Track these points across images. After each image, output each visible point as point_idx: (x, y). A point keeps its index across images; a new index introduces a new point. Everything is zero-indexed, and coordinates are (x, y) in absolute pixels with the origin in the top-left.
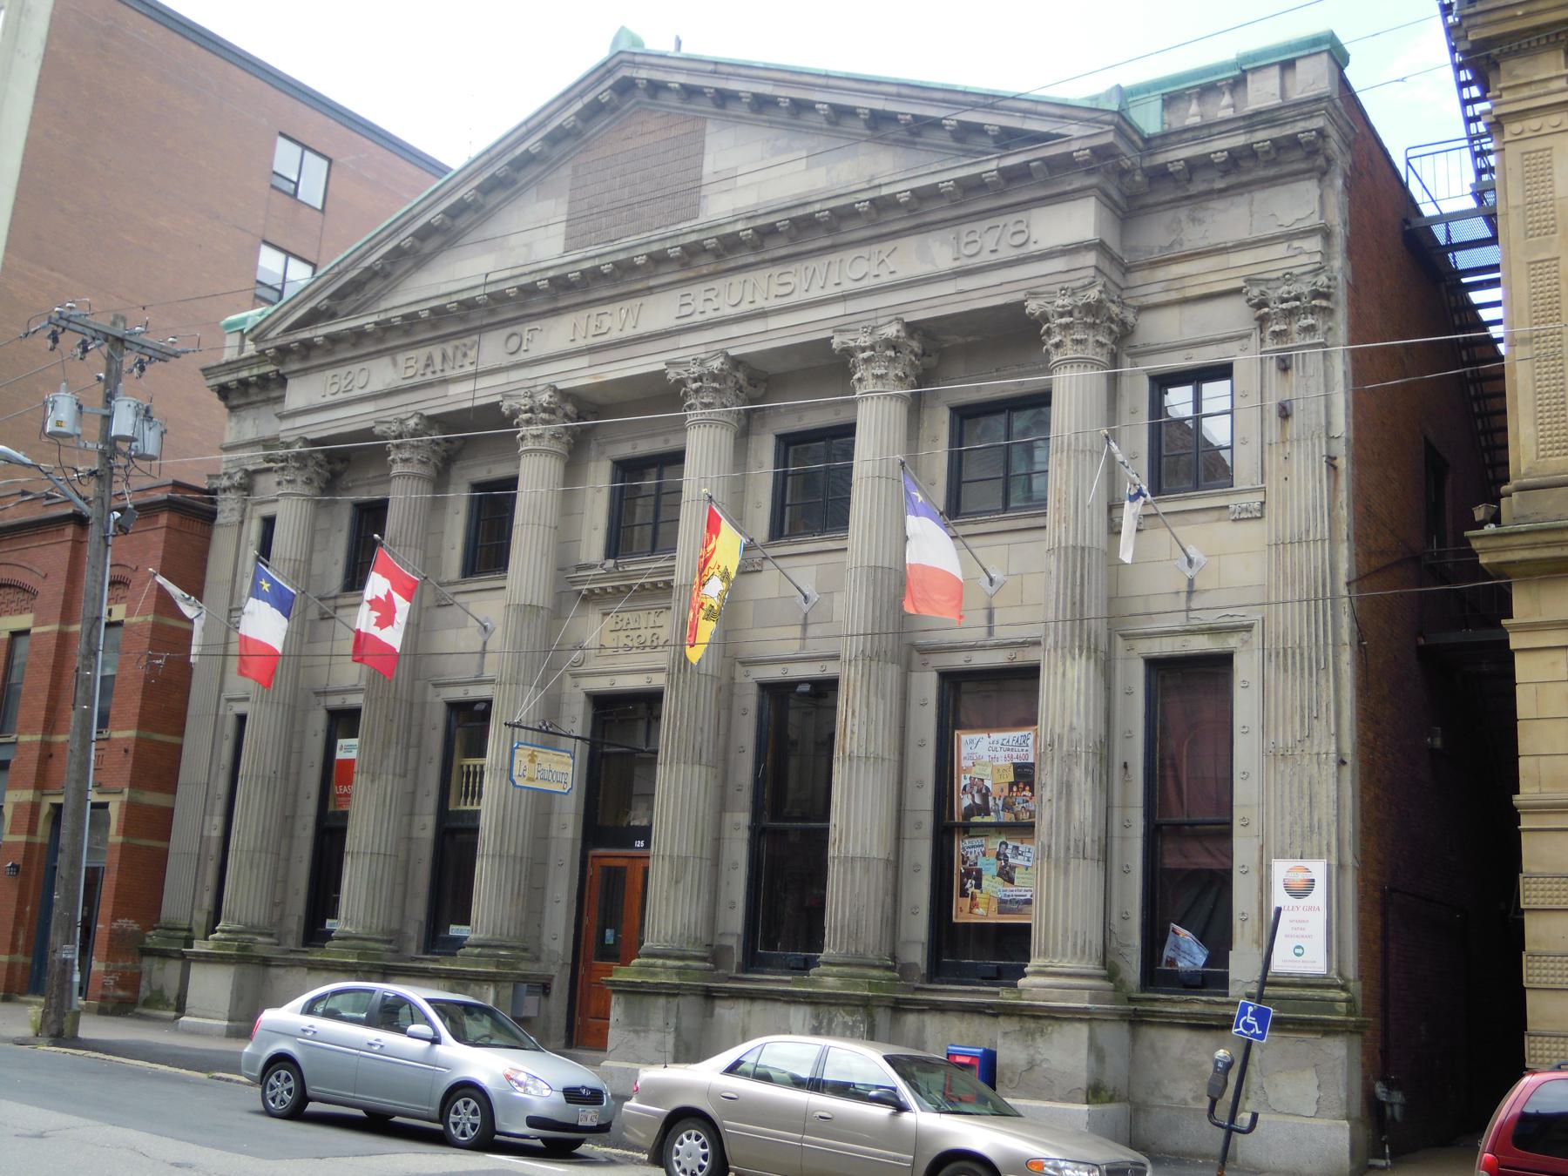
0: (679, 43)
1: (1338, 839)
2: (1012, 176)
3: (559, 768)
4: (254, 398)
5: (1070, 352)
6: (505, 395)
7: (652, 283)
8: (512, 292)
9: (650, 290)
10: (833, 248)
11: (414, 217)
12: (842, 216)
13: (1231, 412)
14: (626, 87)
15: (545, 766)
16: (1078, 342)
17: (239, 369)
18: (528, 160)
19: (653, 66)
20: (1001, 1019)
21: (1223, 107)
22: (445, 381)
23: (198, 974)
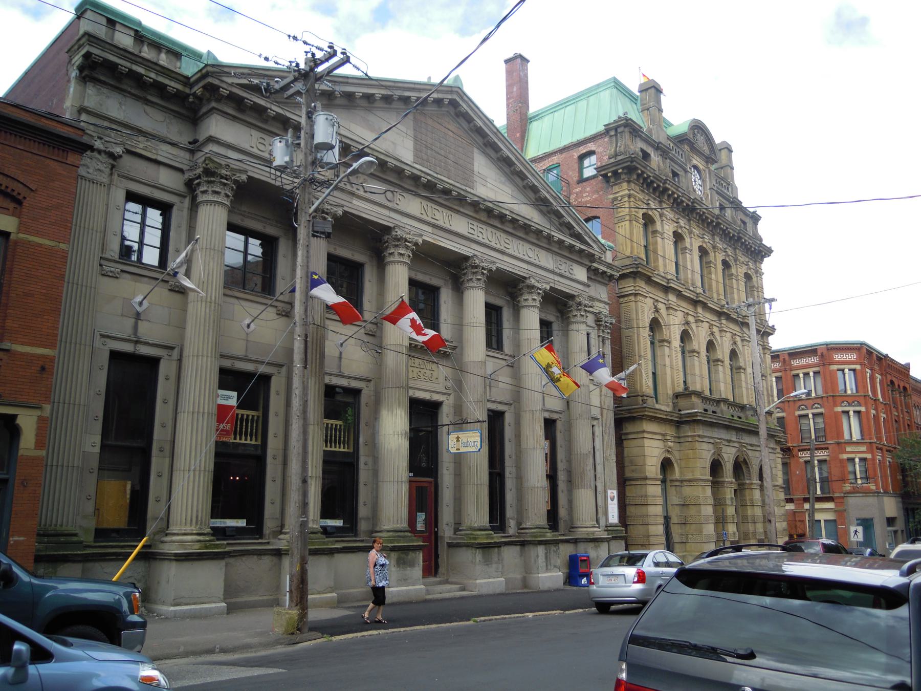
0: (430, 78)
1: (552, 477)
2: (571, 248)
3: (472, 439)
4: (124, 87)
5: (397, 258)
6: (399, 227)
7: (462, 210)
8: (407, 173)
9: (458, 212)
10: (234, 118)
11: (347, 83)
12: (502, 217)
13: (124, 219)
14: (454, 104)
15: (465, 440)
16: (401, 254)
17: (136, 63)
18: (406, 100)
19: (469, 106)
20: (263, 557)
21: (163, 59)
22: (353, 194)
23: (172, 578)
